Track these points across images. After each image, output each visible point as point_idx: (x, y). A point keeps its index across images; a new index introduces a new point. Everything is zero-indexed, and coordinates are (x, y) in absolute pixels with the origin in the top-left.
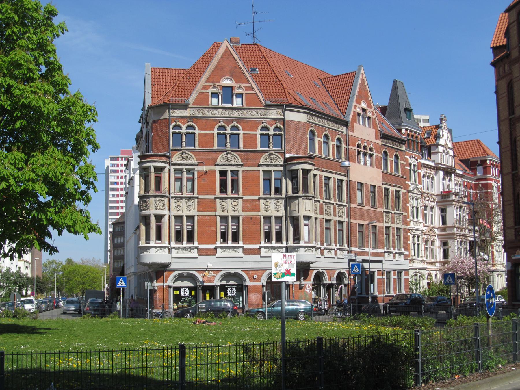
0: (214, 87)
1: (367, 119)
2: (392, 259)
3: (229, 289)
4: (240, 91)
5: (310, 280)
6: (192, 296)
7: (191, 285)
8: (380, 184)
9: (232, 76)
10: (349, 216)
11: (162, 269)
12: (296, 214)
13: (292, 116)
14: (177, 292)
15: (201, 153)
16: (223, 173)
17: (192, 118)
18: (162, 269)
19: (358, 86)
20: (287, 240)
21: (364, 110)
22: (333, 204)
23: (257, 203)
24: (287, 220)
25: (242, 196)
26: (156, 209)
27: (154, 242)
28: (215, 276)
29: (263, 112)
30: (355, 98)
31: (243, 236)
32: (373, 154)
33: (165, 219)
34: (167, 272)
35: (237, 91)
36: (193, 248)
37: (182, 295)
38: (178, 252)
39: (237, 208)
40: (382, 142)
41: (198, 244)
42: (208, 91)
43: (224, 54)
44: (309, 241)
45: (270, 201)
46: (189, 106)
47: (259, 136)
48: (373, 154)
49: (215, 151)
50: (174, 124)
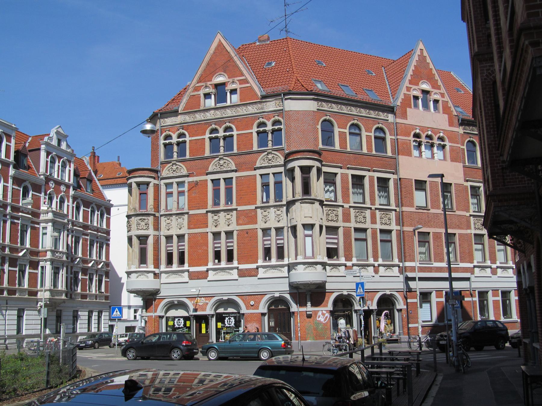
0: (206, 87)
1: (432, 102)
2: (491, 275)
3: (227, 319)
4: (234, 86)
5: (327, 306)
6: (187, 327)
8: (461, 181)
9: (225, 72)
10: (400, 221)
11: (151, 297)
13: (292, 105)
15: (192, 162)
16: (215, 182)
17: (183, 125)
18: (151, 297)
19: (414, 63)
21: (425, 92)
22: (370, 208)
23: (253, 213)
26: (138, 229)
28: (207, 304)
29: (259, 106)
30: (409, 77)
31: (238, 254)
32: (445, 145)
35: (230, 87)
36: (183, 272)
37: (177, 326)
40: (464, 129)
41: (154, 268)
42: (199, 93)
43: (217, 49)
44: (313, 256)
45: (268, 210)
46: (180, 112)
47: (255, 135)
48: (445, 145)
49: (207, 158)
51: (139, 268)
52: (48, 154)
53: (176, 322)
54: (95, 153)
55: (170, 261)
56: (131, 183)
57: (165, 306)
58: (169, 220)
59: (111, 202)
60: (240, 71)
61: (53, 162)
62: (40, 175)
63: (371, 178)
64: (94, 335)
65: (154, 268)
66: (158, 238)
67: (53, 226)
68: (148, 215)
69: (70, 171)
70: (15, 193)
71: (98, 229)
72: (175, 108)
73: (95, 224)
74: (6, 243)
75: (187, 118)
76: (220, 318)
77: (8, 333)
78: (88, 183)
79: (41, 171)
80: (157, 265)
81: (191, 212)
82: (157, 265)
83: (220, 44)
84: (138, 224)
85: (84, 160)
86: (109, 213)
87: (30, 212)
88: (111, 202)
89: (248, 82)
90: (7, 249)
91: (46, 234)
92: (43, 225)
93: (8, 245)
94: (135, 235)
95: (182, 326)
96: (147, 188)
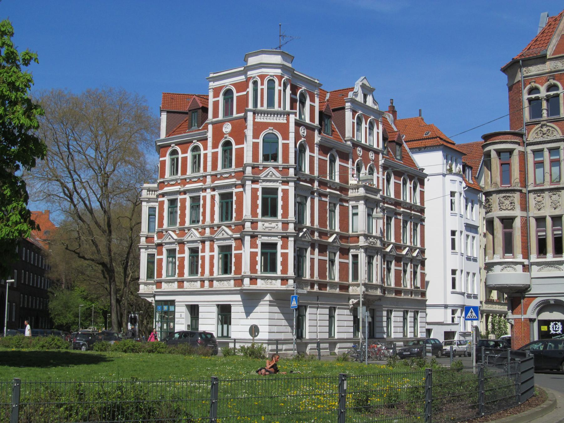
11: (518, 295)
14: (544, 328)
17: (553, 74)
18: (518, 295)
25: (520, 188)
26: (501, 209)
27: (552, 255)
33: (517, 224)
34: (526, 299)
37: (552, 332)
38: (540, 269)
39: (558, 204)
41: (523, 258)
46: (548, 57)
50: (528, 87)
51: (504, 258)
52: (354, 112)
53: (551, 327)
54: (394, 107)
55: (542, 250)
56: (490, 151)
57: (537, 307)
58: (540, 197)
59: (424, 172)
61: (359, 123)
62: (346, 141)
64: (410, 340)
65: (523, 258)
66: (526, 220)
67: (366, 204)
68: (514, 191)
69: (378, 133)
70: (322, 163)
71: (411, 207)
72: (542, 53)
73: (408, 201)
74: (315, 227)
77: (320, 336)
78: (398, 147)
79: (346, 136)
80: (526, 255)
82: (526, 255)
84: (501, 203)
85: (388, 118)
86: (422, 184)
87: (338, 188)
88: (424, 172)
90: (316, 234)
91: (356, 214)
92: (352, 203)
93: (317, 230)
94: (498, 217)
95: (559, 332)
96: (510, 157)
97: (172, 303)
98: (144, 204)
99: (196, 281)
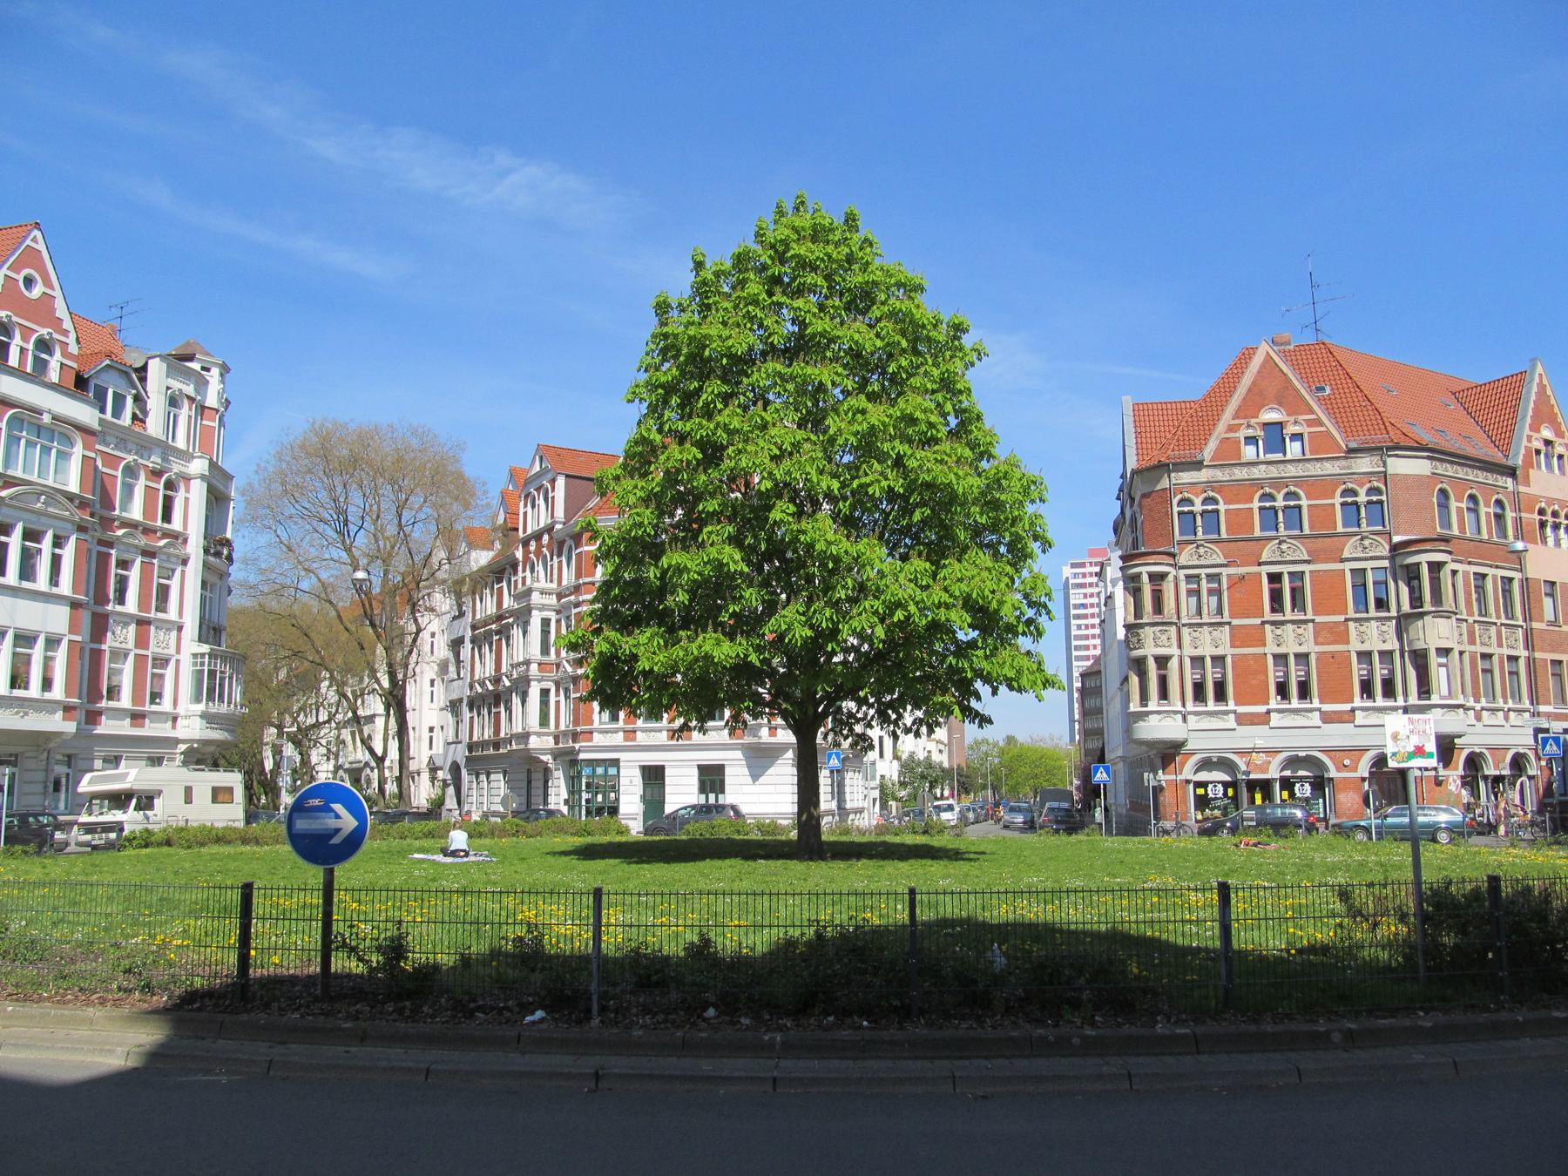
0: (1249, 426)
4: (1296, 429)
7: (1227, 778)
12: (1419, 645)
13: (1404, 466)
14: (1201, 791)
16: (1275, 578)
17: (1211, 484)
19: (1533, 397)
20: (1405, 694)
21: (1548, 443)
24: (1402, 656)
26: (1157, 645)
29: (1344, 463)
35: (1291, 429)
36: (1226, 713)
43: (1263, 366)
47: (1338, 507)
49: (1258, 539)
50: (1179, 497)
60: (1308, 404)
63: (1494, 577)
75: (1219, 475)
76: (1287, 784)
81: (1235, 622)
83: (1268, 357)
89: (1321, 424)
97: (615, 763)
98: (534, 612)
99: (660, 731)
